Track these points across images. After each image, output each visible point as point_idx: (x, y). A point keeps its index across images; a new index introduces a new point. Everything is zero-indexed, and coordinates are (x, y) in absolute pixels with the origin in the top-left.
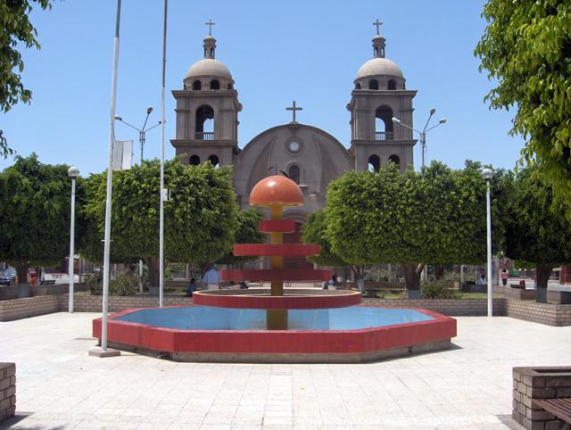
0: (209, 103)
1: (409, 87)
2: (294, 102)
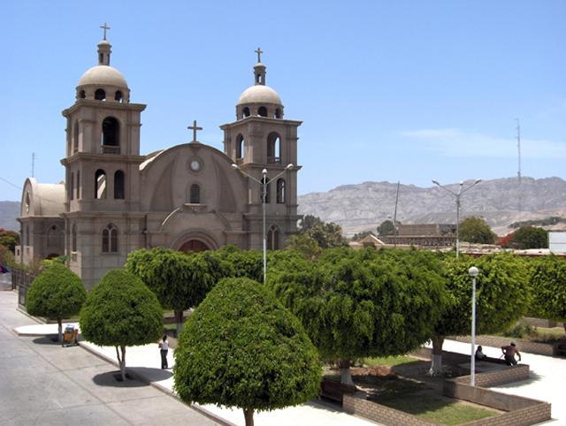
0: (116, 115)
1: (134, 99)
2: (195, 122)
